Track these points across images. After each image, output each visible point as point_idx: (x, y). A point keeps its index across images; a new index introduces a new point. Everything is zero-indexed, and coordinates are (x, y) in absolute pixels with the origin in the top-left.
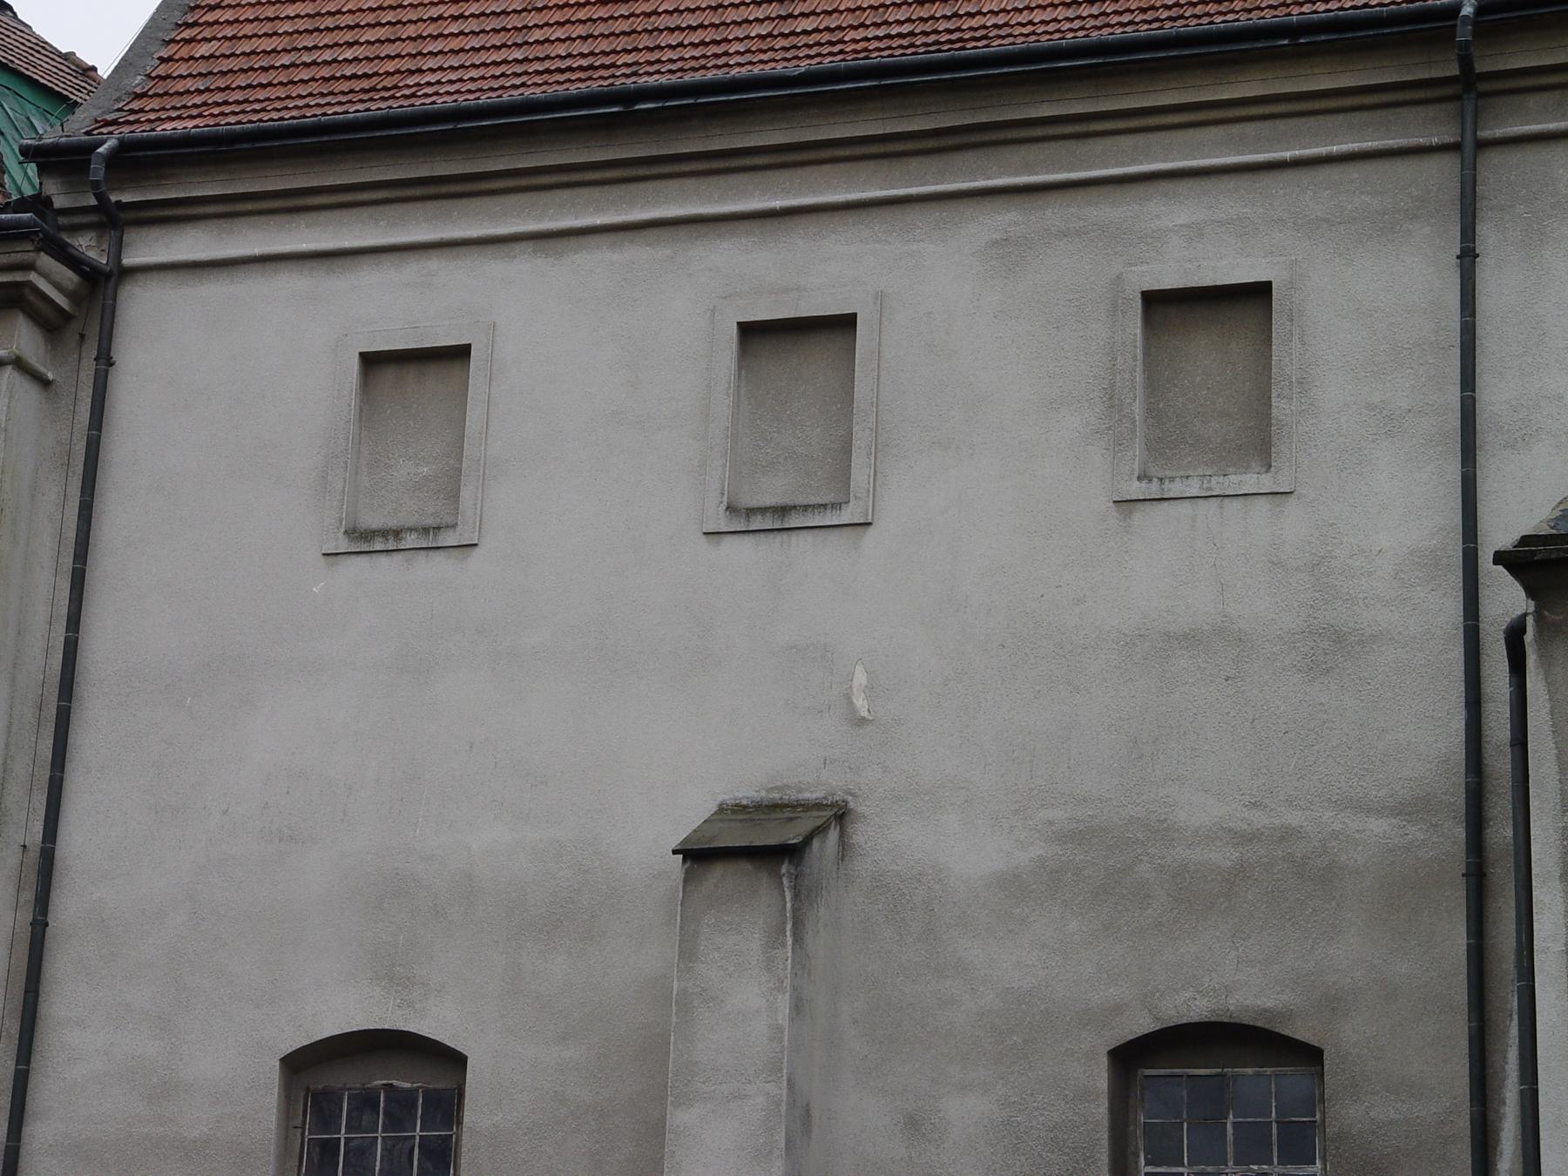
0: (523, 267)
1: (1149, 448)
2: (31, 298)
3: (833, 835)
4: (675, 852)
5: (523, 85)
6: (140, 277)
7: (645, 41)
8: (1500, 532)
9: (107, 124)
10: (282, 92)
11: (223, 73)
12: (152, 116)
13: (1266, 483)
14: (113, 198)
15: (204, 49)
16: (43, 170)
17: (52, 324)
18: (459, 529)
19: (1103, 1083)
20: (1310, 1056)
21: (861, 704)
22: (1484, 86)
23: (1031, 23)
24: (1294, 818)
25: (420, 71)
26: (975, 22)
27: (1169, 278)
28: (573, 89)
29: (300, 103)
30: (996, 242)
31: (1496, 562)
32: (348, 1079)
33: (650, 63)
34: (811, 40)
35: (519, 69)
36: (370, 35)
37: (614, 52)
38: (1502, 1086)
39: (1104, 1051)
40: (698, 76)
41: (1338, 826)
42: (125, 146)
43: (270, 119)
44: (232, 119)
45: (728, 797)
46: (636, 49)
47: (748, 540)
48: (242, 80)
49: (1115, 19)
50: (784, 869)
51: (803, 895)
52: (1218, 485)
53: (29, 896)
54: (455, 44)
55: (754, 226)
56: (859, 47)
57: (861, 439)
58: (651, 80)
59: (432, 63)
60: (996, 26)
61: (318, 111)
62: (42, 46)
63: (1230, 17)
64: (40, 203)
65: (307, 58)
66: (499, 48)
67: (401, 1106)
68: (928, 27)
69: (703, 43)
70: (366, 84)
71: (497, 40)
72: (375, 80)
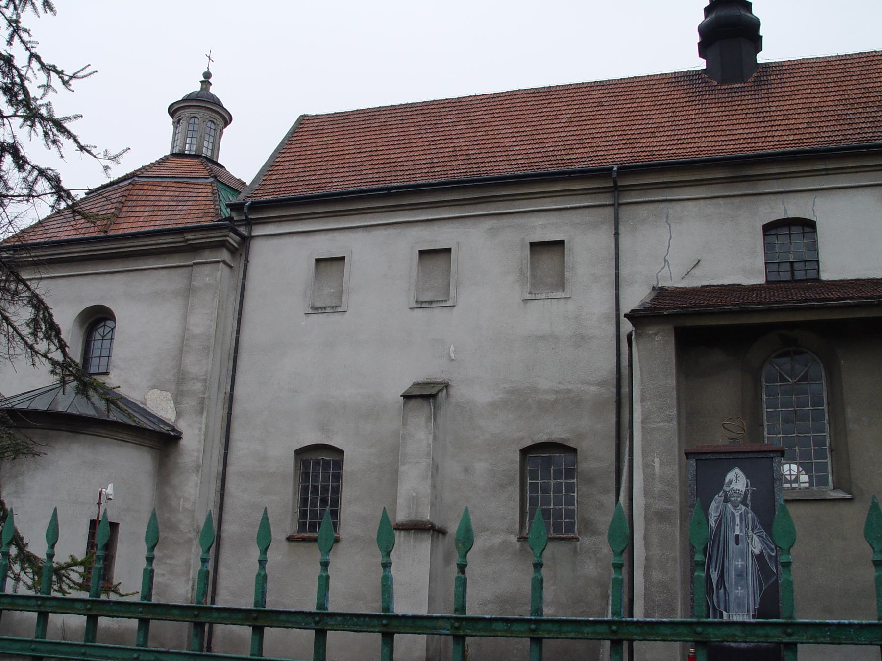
0: (360, 235)
1: (531, 285)
2: (228, 244)
3: (445, 391)
4: (401, 396)
5: (360, 186)
6: (257, 238)
7: (394, 174)
8: (626, 309)
9: (248, 197)
10: (295, 188)
11: (279, 183)
12: (260, 195)
13: (563, 295)
14: (250, 217)
15: (275, 177)
16: (231, 210)
17: (233, 251)
18: (342, 307)
19: (518, 459)
20: (574, 451)
21: (452, 355)
22: (620, 189)
23: (499, 169)
24: (570, 387)
25: (332, 182)
26: (484, 169)
27: (537, 239)
28: (374, 187)
29: (300, 191)
30: (489, 229)
31: (625, 317)
32: (312, 457)
33: (395, 180)
34: (439, 173)
35: (359, 181)
36: (319, 173)
37: (385, 177)
38: (624, 457)
39: (518, 450)
40: (408, 183)
41: (582, 389)
42: (253, 203)
43: (292, 195)
44: (281, 196)
45: (416, 381)
46: (391, 176)
47: (422, 310)
48: (284, 185)
49: (522, 169)
50: (431, 400)
51: (436, 408)
52: (551, 295)
53: (227, 406)
54: (342, 175)
55: (423, 224)
56: (452, 175)
57: (452, 282)
58: (395, 184)
59: (336, 180)
60: (490, 170)
61: (305, 193)
62: (232, 177)
63: (553, 169)
64: (230, 219)
65: (302, 179)
66: (354, 176)
67: (326, 464)
68: (471, 170)
69: (410, 174)
70: (318, 186)
71: (353, 174)
72: (320, 185)
